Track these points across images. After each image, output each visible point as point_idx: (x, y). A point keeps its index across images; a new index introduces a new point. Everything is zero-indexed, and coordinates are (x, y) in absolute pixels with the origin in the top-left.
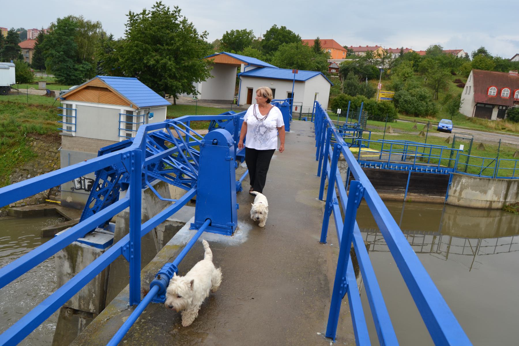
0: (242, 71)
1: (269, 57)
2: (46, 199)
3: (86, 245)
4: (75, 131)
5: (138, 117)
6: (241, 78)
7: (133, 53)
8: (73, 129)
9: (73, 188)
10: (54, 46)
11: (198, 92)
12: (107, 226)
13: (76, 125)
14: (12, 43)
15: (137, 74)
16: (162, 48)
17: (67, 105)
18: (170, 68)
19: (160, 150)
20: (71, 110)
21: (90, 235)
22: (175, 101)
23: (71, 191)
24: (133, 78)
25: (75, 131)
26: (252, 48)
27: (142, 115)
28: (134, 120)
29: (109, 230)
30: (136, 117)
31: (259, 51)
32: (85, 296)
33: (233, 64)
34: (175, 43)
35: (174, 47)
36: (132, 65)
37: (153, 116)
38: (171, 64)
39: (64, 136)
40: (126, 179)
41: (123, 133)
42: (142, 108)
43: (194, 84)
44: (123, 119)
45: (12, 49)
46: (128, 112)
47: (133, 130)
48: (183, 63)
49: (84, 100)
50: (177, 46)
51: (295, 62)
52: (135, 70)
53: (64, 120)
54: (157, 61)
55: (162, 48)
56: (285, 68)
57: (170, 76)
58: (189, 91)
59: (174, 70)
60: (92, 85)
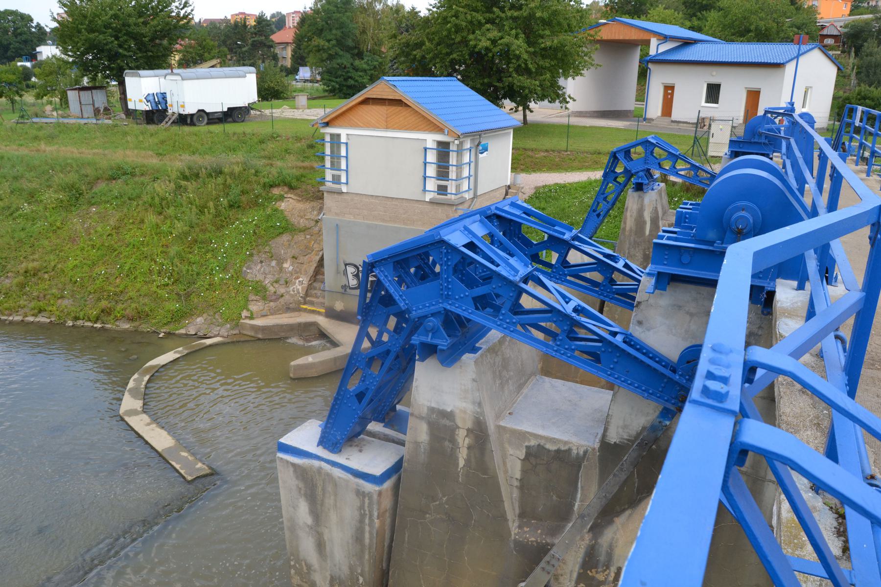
0: (652, 51)
1: (696, 23)
2: (301, 303)
3: (343, 472)
4: (347, 183)
5: (460, 152)
6: (650, 65)
7: (449, 31)
8: (343, 180)
9: (345, 285)
10: (320, 32)
11: (569, 97)
12: (392, 414)
13: (347, 171)
14: (261, 35)
15: (455, 71)
16: (503, 15)
17: (332, 135)
18: (518, 52)
19: (515, 258)
20: (339, 144)
21: (351, 446)
22: (525, 116)
23: (343, 291)
24: (449, 78)
25: (347, 183)
26: (665, 9)
27: (467, 149)
28: (453, 159)
29: (396, 428)
30: (455, 154)
31: (678, 14)
32: (343, 576)
33: (635, 40)
34: (527, 5)
35: (525, 13)
36: (448, 54)
37: (486, 150)
38: (519, 45)
39: (328, 192)
40: (430, 334)
41: (431, 185)
42: (467, 135)
43: (561, 81)
44: (432, 157)
45: (262, 45)
46: (440, 143)
47: (450, 178)
48: (543, 43)
49: (362, 125)
50: (531, 9)
51: (752, 27)
52: (453, 63)
53: (328, 164)
54: (494, 42)
55: (503, 15)
56: (733, 41)
57: (518, 70)
58: (554, 96)
59: (525, 56)
60: (374, 97)
